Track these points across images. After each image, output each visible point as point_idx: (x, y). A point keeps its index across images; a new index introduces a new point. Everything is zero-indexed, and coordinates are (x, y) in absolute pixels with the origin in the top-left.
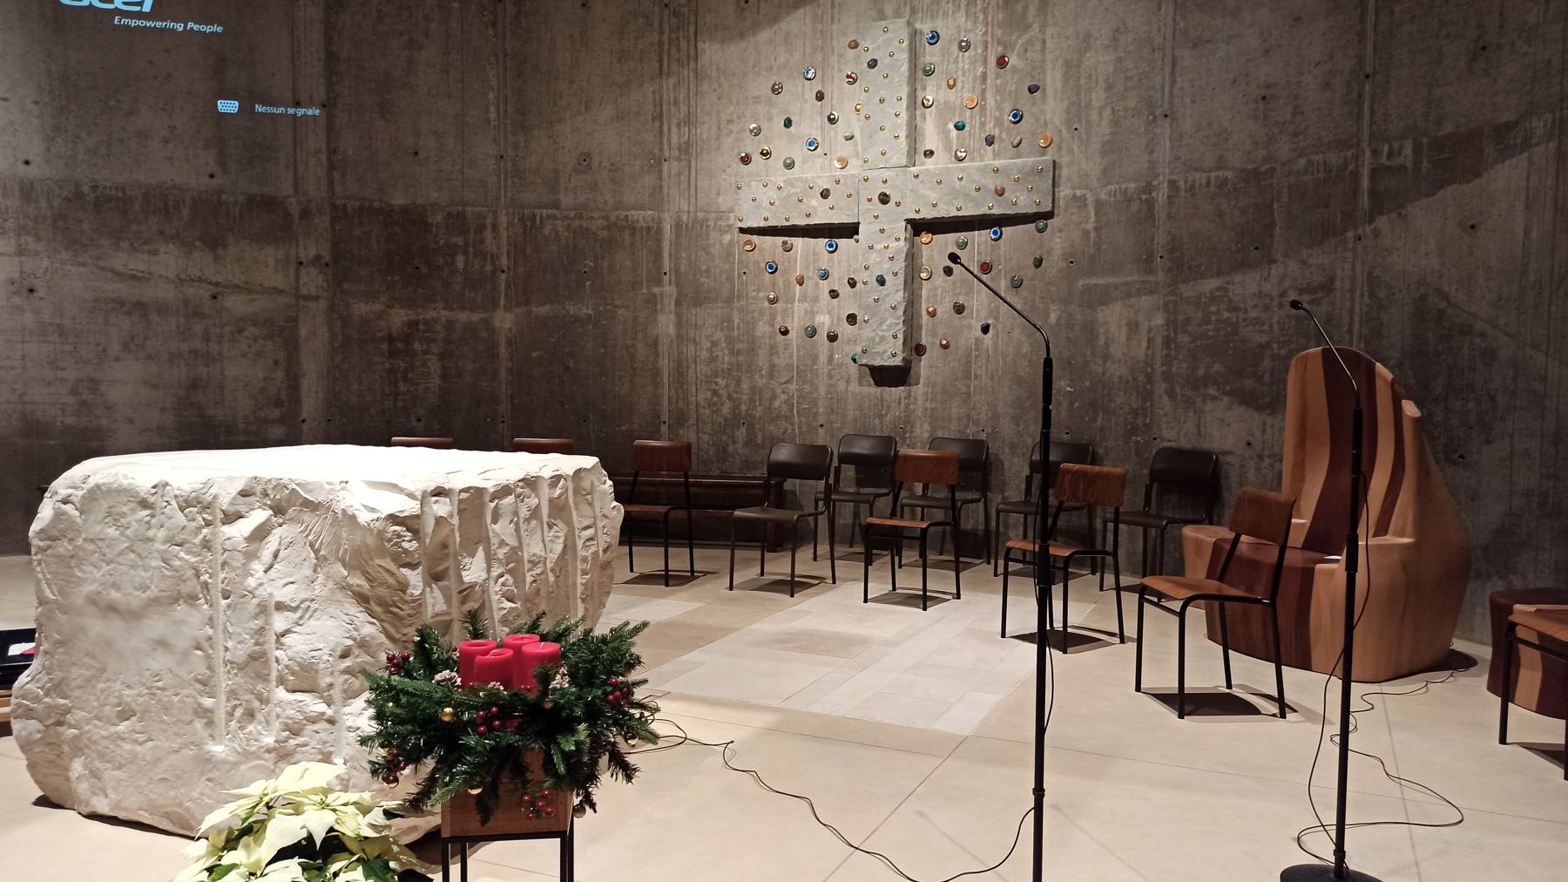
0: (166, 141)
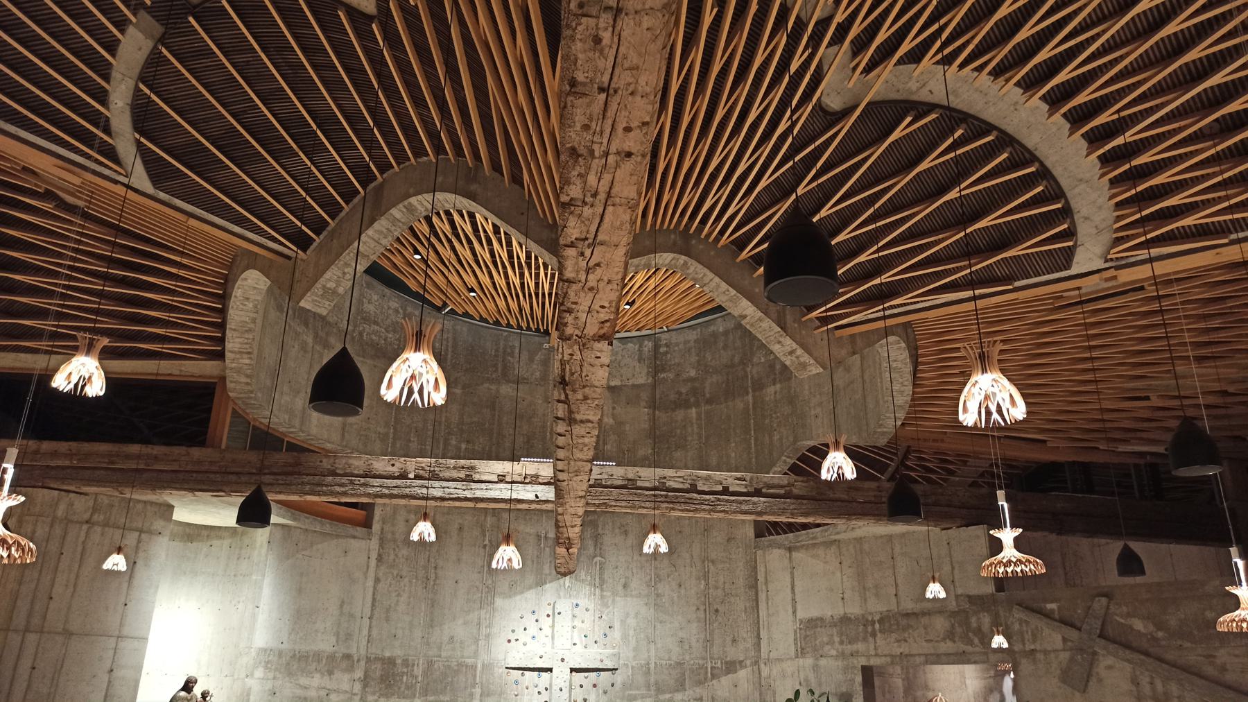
0: (323, 633)
